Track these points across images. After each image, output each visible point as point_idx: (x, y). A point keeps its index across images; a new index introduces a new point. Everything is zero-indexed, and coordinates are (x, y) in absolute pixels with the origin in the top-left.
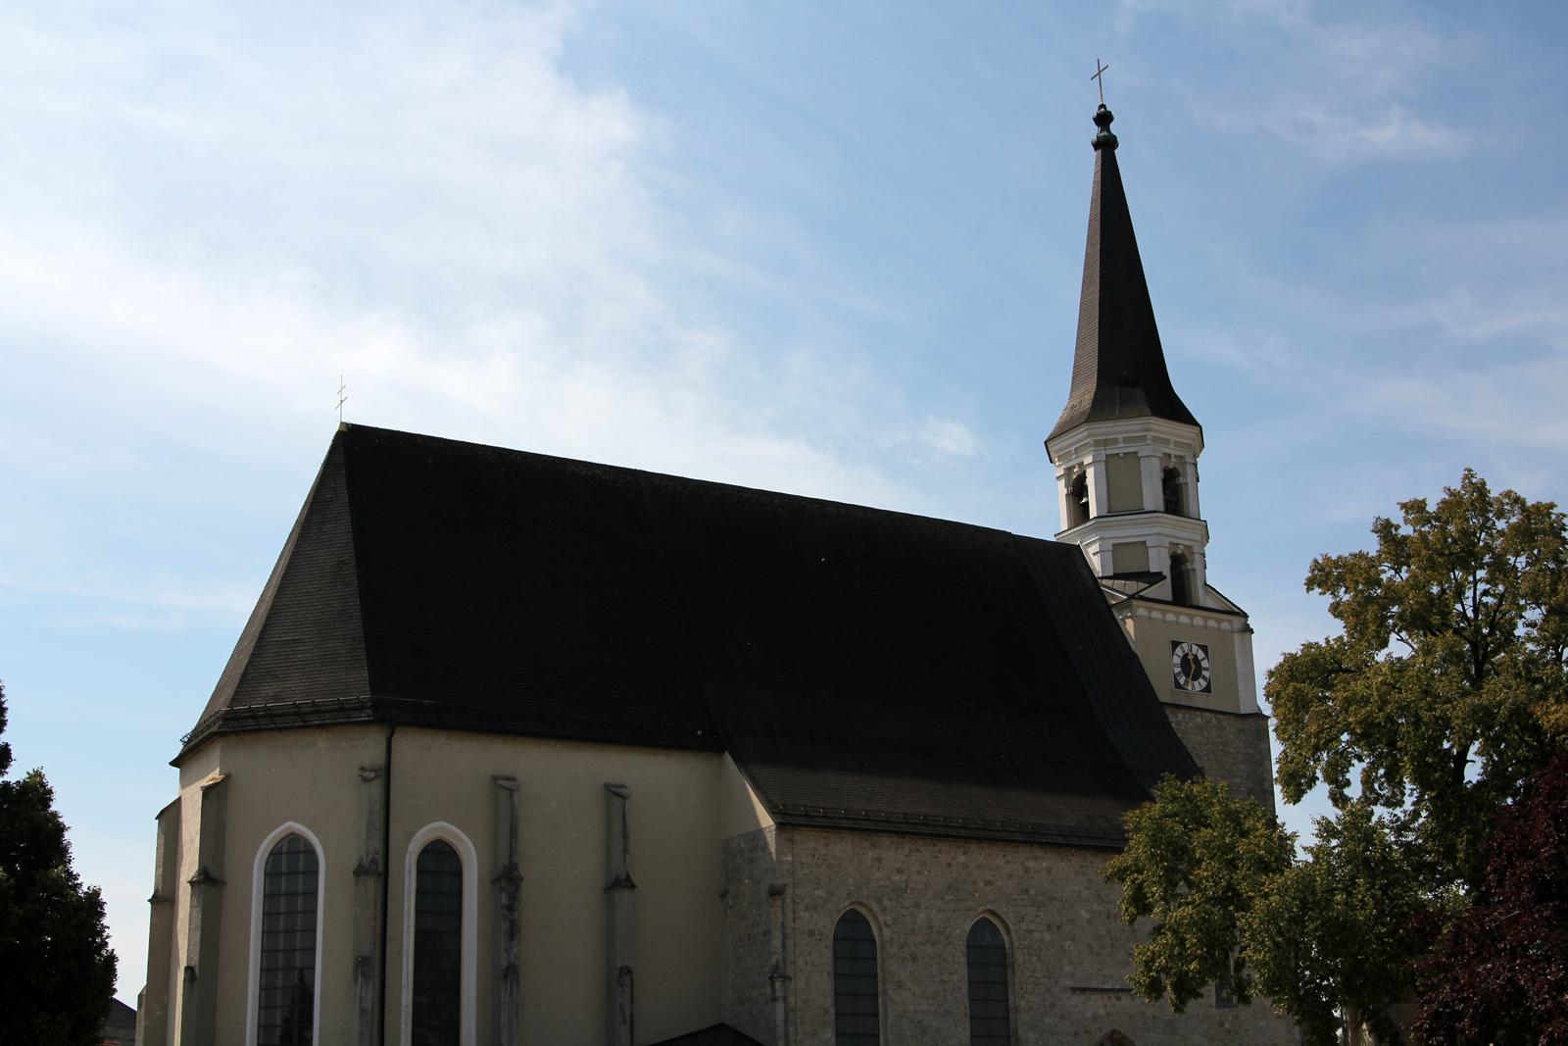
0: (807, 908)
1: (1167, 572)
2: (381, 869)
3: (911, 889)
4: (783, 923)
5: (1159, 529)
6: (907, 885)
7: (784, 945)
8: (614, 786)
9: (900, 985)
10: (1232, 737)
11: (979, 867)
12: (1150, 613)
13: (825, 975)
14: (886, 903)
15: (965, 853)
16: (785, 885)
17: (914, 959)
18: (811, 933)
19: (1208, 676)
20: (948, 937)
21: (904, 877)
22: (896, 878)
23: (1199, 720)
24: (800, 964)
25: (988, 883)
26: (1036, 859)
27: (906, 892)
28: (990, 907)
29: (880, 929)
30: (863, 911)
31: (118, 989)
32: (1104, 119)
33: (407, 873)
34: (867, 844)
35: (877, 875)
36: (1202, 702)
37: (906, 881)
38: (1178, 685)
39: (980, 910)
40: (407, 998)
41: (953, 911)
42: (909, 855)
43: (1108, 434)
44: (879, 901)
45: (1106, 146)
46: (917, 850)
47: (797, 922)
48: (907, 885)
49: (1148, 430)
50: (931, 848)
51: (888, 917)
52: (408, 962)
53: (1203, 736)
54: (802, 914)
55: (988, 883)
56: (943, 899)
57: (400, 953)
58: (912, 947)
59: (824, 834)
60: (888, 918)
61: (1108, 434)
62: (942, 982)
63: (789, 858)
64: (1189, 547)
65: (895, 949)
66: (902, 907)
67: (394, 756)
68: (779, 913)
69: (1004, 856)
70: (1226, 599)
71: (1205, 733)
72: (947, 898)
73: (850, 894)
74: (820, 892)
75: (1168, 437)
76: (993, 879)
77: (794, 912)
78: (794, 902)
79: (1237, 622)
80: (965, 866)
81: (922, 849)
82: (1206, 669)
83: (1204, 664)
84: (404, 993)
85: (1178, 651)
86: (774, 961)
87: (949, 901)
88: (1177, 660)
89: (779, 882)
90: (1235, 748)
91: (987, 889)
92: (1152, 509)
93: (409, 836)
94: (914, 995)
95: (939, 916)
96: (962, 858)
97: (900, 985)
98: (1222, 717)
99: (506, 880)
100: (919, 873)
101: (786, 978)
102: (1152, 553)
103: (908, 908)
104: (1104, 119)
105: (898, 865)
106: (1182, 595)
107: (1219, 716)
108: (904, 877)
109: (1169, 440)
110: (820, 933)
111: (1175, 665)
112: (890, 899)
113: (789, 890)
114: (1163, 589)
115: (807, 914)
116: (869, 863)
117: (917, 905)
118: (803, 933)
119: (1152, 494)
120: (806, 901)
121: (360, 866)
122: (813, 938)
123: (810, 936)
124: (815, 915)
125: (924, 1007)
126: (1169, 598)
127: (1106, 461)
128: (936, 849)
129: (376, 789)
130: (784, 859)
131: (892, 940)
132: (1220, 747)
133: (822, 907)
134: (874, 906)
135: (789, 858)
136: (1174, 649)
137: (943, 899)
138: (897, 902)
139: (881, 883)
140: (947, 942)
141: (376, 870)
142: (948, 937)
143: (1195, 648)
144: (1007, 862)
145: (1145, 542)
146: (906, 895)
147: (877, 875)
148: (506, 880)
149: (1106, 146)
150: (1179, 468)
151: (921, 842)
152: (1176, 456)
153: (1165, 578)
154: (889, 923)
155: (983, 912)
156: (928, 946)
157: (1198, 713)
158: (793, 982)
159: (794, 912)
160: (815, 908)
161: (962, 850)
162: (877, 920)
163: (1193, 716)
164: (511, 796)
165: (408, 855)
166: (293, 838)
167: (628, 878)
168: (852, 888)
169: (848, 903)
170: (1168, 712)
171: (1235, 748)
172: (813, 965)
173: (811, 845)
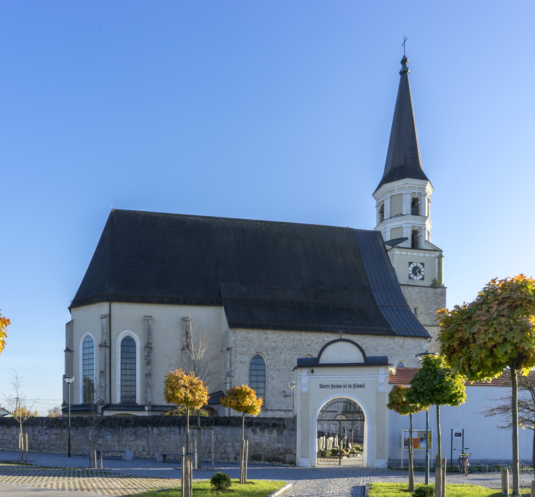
0: (240, 354)
1: (410, 237)
2: (108, 344)
3: (279, 348)
4: (230, 359)
5: (408, 221)
6: (277, 346)
7: (230, 366)
8: (185, 318)
9: (273, 379)
10: (431, 295)
11: (305, 340)
12: (430, 255)
13: (246, 375)
14: (269, 352)
15: (300, 335)
16: (232, 347)
17: (279, 370)
18: (241, 362)
19: (423, 274)
20: (292, 363)
21: (276, 344)
22: (274, 344)
23: (418, 290)
24: (237, 371)
25: (308, 345)
26: (328, 337)
27: (277, 349)
28: (309, 353)
29: (267, 361)
30: (261, 355)
31: (387, 409)
32: (404, 61)
33: (117, 346)
34: (262, 333)
35: (266, 343)
36: (420, 283)
37: (277, 345)
38: (410, 278)
39: (305, 354)
40: (118, 383)
41: (295, 355)
42: (279, 337)
43: (392, 188)
44: (267, 352)
45: (404, 73)
46: (282, 335)
47: (236, 358)
48: (277, 346)
49: (407, 184)
50: (287, 334)
51: (270, 357)
52: (118, 373)
53: (419, 296)
54: (238, 356)
55: (308, 345)
56: (291, 351)
57: (115, 370)
58: (278, 366)
59: (247, 330)
60: (270, 357)
61: (392, 188)
62: (289, 377)
63: (234, 338)
64: (421, 227)
65: (272, 367)
66: (275, 354)
67: (112, 311)
68: (229, 356)
69: (315, 336)
70: (434, 245)
71: (420, 294)
72: (292, 350)
73: (256, 350)
74: (245, 349)
75: (415, 186)
76: (310, 344)
77: (235, 355)
78: (235, 352)
79: (437, 254)
80: (300, 340)
81: (284, 334)
82: (423, 272)
83: (422, 270)
84: (117, 382)
85: (412, 266)
86: (227, 371)
87: (293, 352)
88: (411, 269)
89: (230, 346)
90: (431, 299)
91: (308, 347)
92: (406, 214)
93: (118, 335)
94: (278, 382)
95: (289, 356)
96: (299, 337)
97: (273, 379)
98: (427, 288)
99: (148, 347)
100: (282, 342)
101: (230, 376)
102: (405, 230)
103: (278, 354)
104: (404, 61)
105: (274, 340)
106: (415, 245)
107: (426, 288)
108: (276, 344)
109: (415, 187)
110: (244, 362)
111: (410, 271)
112: (271, 351)
113: (234, 348)
114: (408, 244)
115: (240, 356)
116: (263, 339)
117: (281, 353)
118: (238, 362)
119: (407, 208)
120: (240, 352)
121: (101, 344)
122: (242, 364)
123: (241, 363)
124: (243, 356)
125: (282, 386)
126: (410, 246)
127: (391, 198)
128: (288, 334)
129: (105, 321)
130: (232, 338)
131: (271, 364)
132: (426, 299)
133: (245, 354)
134: (265, 353)
135: (234, 338)
136: (409, 265)
137: (291, 351)
138: (273, 352)
139: (268, 346)
140: (292, 365)
141: (107, 345)
142: (292, 363)
143: (419, 265)
144: (316, 338)
145: (402, 227)
146: (277, 350)
147: (266, 343)
148: (148, 347)
149: (404, 73)
150: (419, 197)
151: (283, 332)
152: (418, 193)
153: (408, 239)
154: (270, 359)
155: (307, 355)
156: (284, 366)
157: (417, 287)
158: (234, 377)
159: (235, 355)
160: (243, 354)
161: (299, 335)
162: (266, 358)
163: (415, 289)
164: (148, 322)
165: (117, 341)
166: (88, 336)
167: (151, 343)
168: (256, 348)
169: (255, 352)
170: (402, 288)
171: (431, 299)
172: (241, 372)
173: (242, 334)
